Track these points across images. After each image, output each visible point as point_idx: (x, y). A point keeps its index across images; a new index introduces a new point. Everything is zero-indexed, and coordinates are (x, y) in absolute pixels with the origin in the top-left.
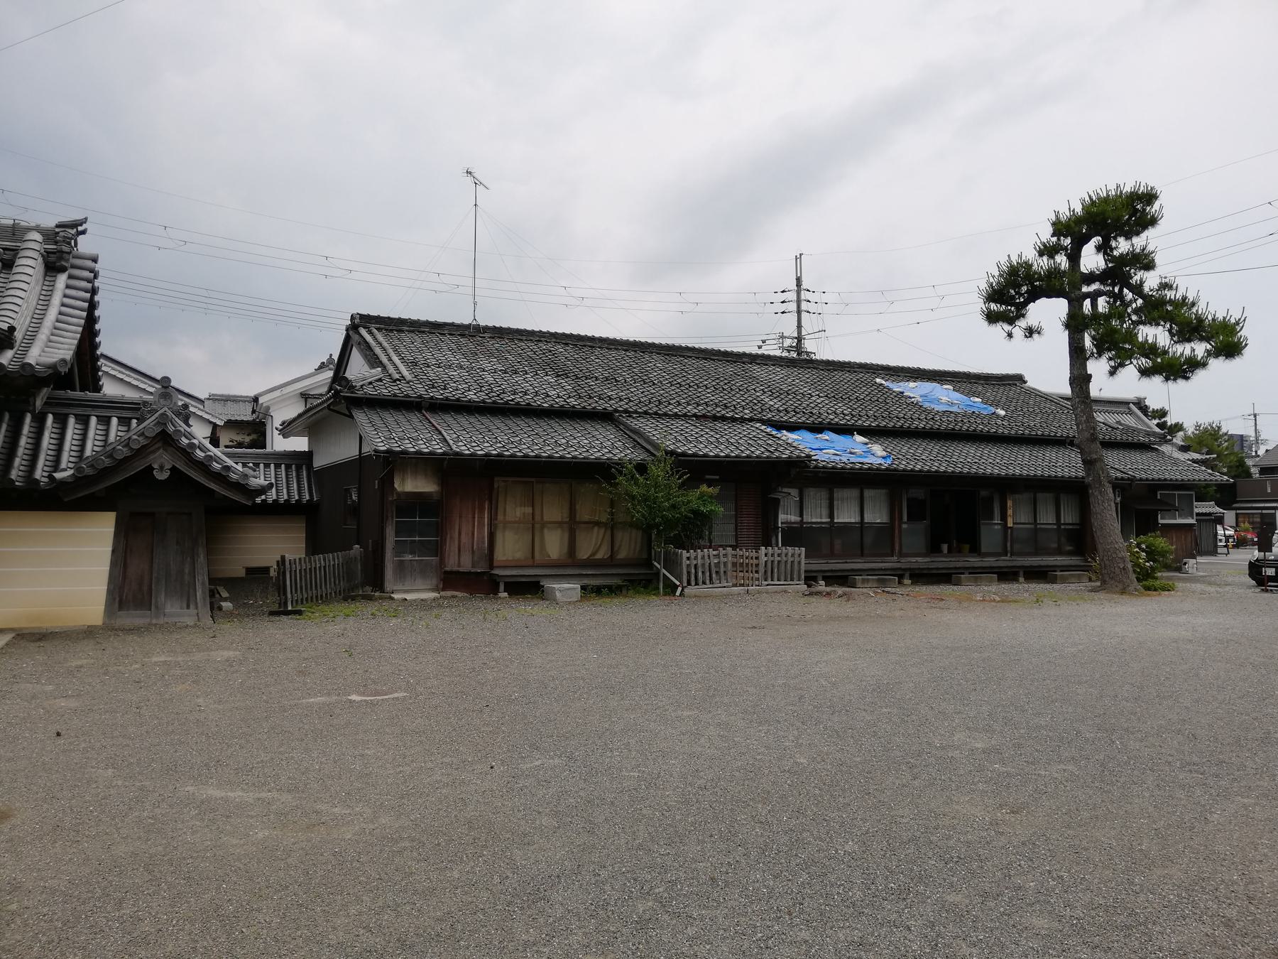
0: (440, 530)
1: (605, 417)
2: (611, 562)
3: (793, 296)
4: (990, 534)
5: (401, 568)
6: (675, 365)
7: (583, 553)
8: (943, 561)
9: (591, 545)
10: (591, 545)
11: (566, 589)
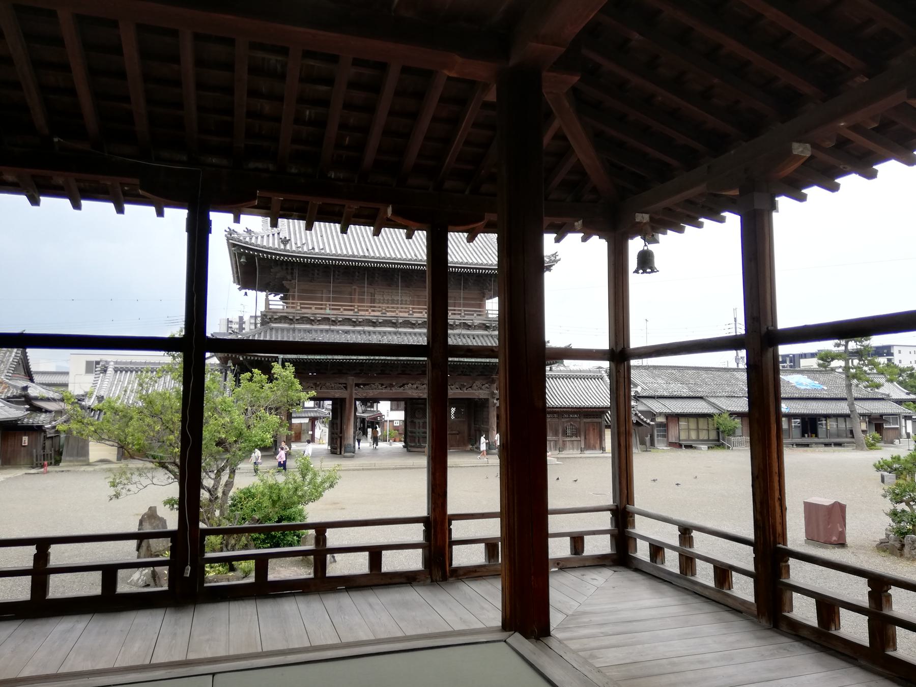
0: (667, 431)
1: (701, 398)
2: (708, 440)
3: (733, 326)
4: (821, 430)
5: (452, 446)
6: (710, 375)
7: (701, 438)
8: (806, 440)
9: (703, 435)
10: (703, 435)
11: (704, 447)
